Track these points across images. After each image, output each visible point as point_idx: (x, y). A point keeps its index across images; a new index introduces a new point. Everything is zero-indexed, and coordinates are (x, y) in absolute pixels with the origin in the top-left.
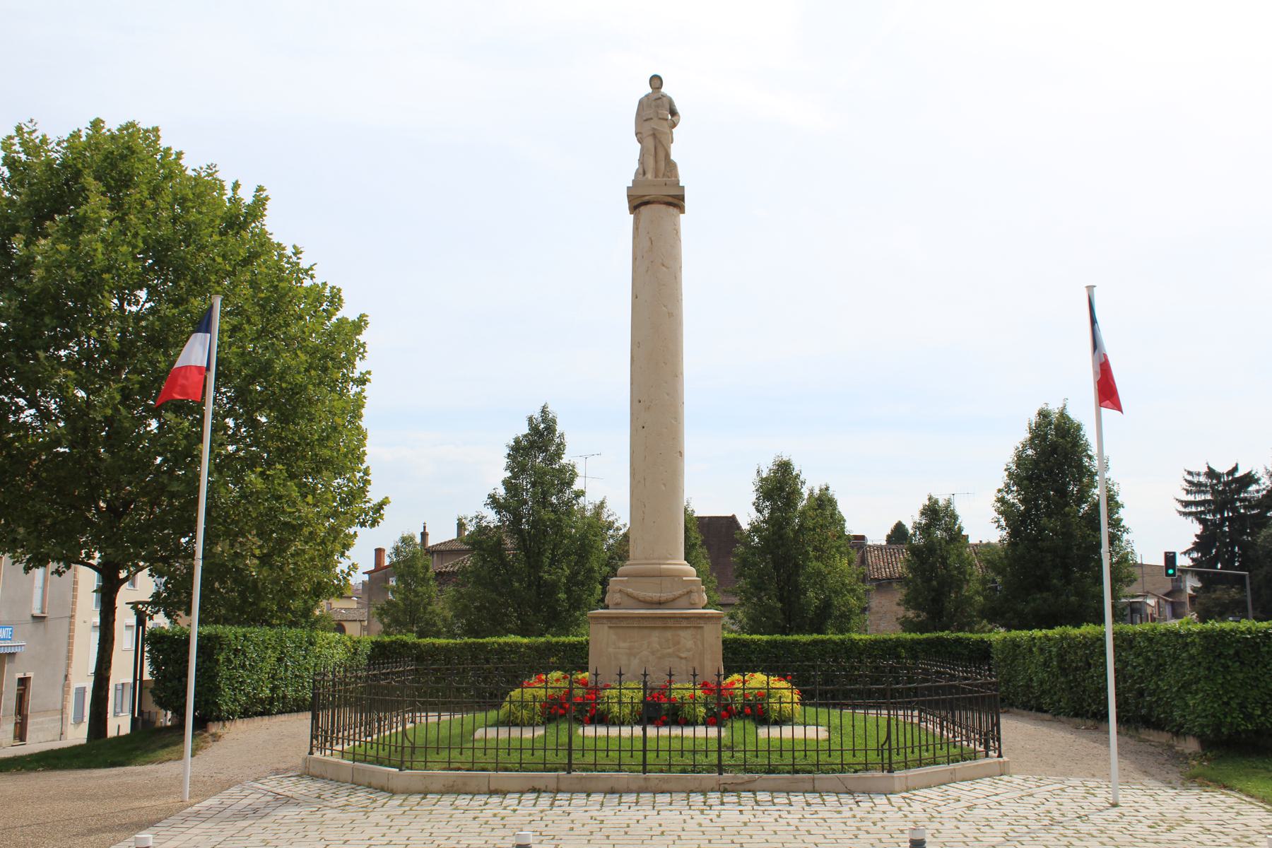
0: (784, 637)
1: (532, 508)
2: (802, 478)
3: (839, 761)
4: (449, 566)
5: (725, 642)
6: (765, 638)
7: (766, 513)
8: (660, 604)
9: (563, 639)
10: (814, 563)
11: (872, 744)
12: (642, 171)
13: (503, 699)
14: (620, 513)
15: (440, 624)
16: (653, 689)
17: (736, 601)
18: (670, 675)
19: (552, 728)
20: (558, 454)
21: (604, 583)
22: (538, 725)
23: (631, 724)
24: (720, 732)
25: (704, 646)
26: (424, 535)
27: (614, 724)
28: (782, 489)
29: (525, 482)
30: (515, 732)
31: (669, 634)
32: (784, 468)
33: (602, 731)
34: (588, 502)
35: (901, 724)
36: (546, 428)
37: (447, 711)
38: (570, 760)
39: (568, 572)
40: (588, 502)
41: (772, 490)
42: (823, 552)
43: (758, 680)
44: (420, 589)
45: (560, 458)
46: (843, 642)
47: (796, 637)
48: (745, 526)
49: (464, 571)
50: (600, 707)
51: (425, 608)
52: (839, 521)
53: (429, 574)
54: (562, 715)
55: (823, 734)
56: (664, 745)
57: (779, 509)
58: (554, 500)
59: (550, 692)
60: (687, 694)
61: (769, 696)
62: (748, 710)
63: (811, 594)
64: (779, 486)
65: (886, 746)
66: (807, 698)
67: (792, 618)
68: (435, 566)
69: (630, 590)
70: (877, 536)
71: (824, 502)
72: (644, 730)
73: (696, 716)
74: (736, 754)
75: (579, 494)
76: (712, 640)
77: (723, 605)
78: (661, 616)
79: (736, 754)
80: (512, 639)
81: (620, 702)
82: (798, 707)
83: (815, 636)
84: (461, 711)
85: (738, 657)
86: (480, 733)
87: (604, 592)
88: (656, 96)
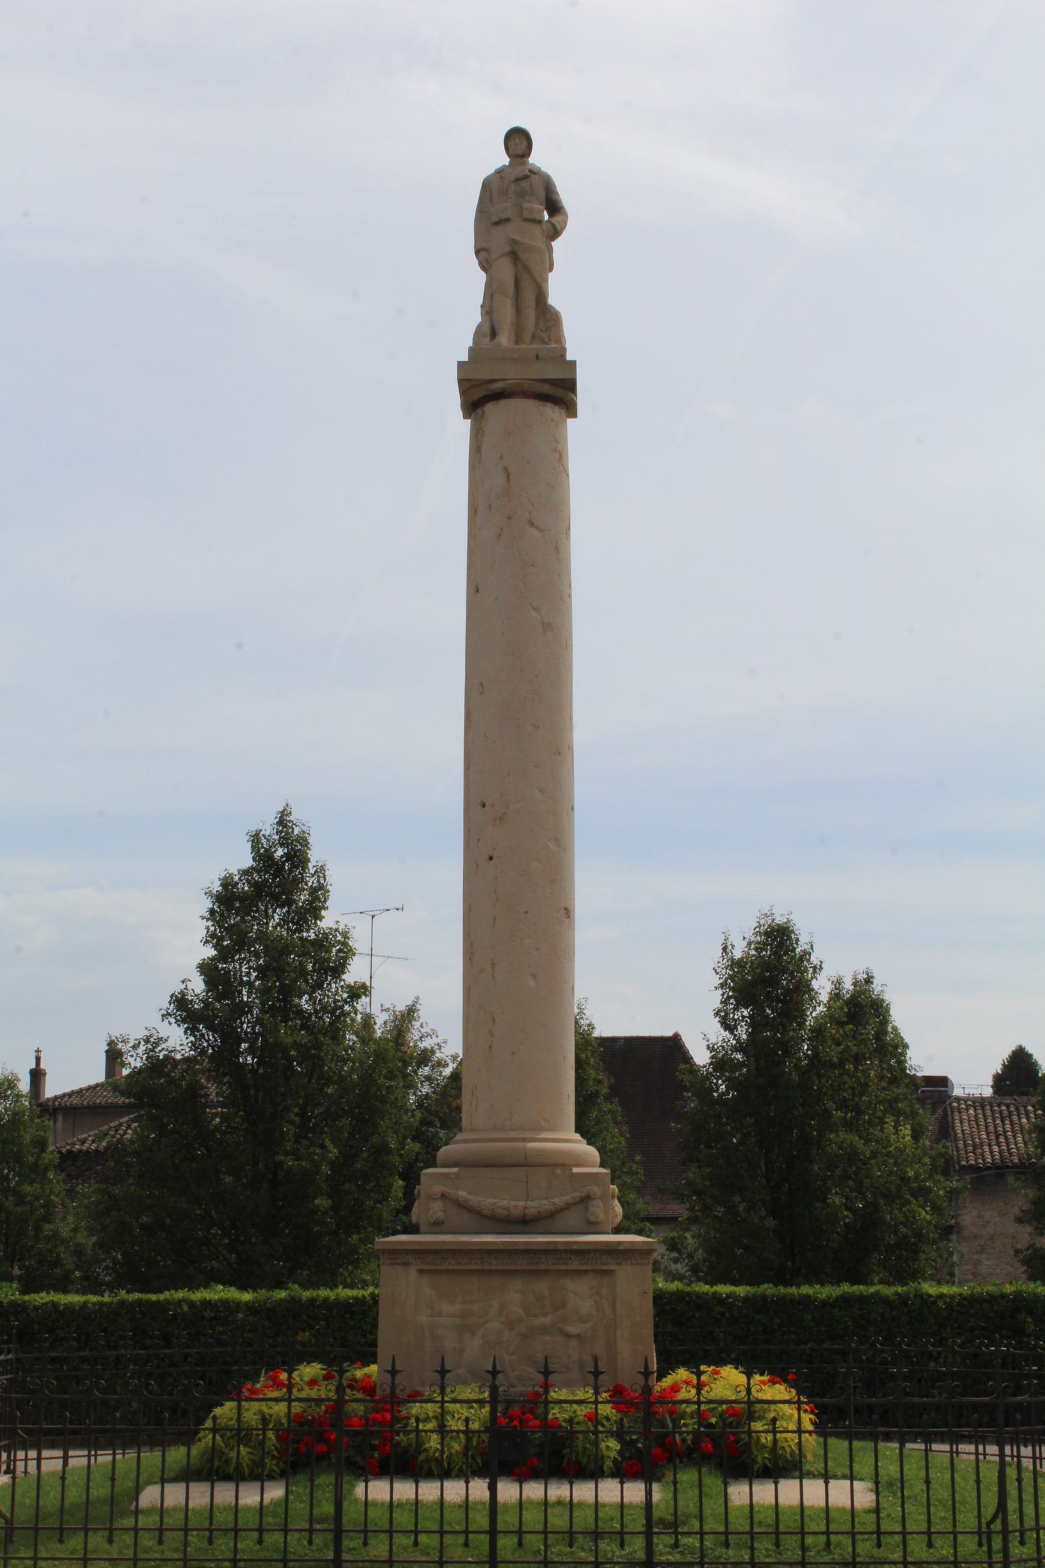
0: (782, 1289)
1: (259, 1021)
2: (814, 959)
3: (897, 1556)
4: (87, 1139)
5: (660, 1299)
6: (742, 1290)
7: (743, 1032)
8: (525, 1223)
9: (324, 1293)
10: (842, 1135)
11: (968, 1520)
12: (488, 331)
13: (201, 1421)
14: (444, 1030)
15: (69, 1261)
16: (509, 1403)
17: (681, 1210)
18: (546, 1373)
19: (301, 1488)
20: (315, 908)
21: (411, 1177)
22: (271, 1477)
23: (466, 1474)
24: (649, 1493)
25: (617, 1317)
26: (37, 1075)
27: (429, 1475)
28: (774, 982)
29: (245, 968)
30: (225, 1493)
31: (542, 1286)
32: (778, 938)
33: (404, 1490)
34: (380, 1008)
35: (1028, 1477)
36: (288, 857)
37: (80, 1446)
38: (338, 1551)
39: (334, 1152)
40: (380, 1008)
41: (753, 984)
42: (859, 1112)
43: (728, 1381)
44: (27, 1188)
45: (318, 917)
46: (903, 1299)
47: (806, 1290)
48: (701, 1057)
49: (117, 1150)
50: (401, 1438)
51: (38, 1229)
52: (891, 1049)
53: (47, 1157)
54: (322, 1457)
55: (864, 1497)
56: (532, 1519)
57: (767, 1023)
58: (304, 1002)
59: (297, 1408)
60: (582, 1411)
61: (752, 1417)
62: (707, 1445)
63: (836, 1200)
64: (767, 974)
65: (997, 1526)
66: (831, 1420)
67: (799, 1251)
68: (61, 1139)
69: (463, 1194)
70: (973, 1077)
71: (862, 1009)
72: (493, 1489)
73: (600, 1458)
74: (684, 1540)
75: (358, 991)
76: (635, 1292)
77: (656, 1221)
78: (529, 1253)
79: (684, 1540)
80: (219, 1293)
81: (442, 1429)
82: (811, 1441)
83: (846, 1288)
84: (111, 1445)
85: (687, 1333)
86: (149, 1496)
87: (410, 1196)
88: (520, 171)
